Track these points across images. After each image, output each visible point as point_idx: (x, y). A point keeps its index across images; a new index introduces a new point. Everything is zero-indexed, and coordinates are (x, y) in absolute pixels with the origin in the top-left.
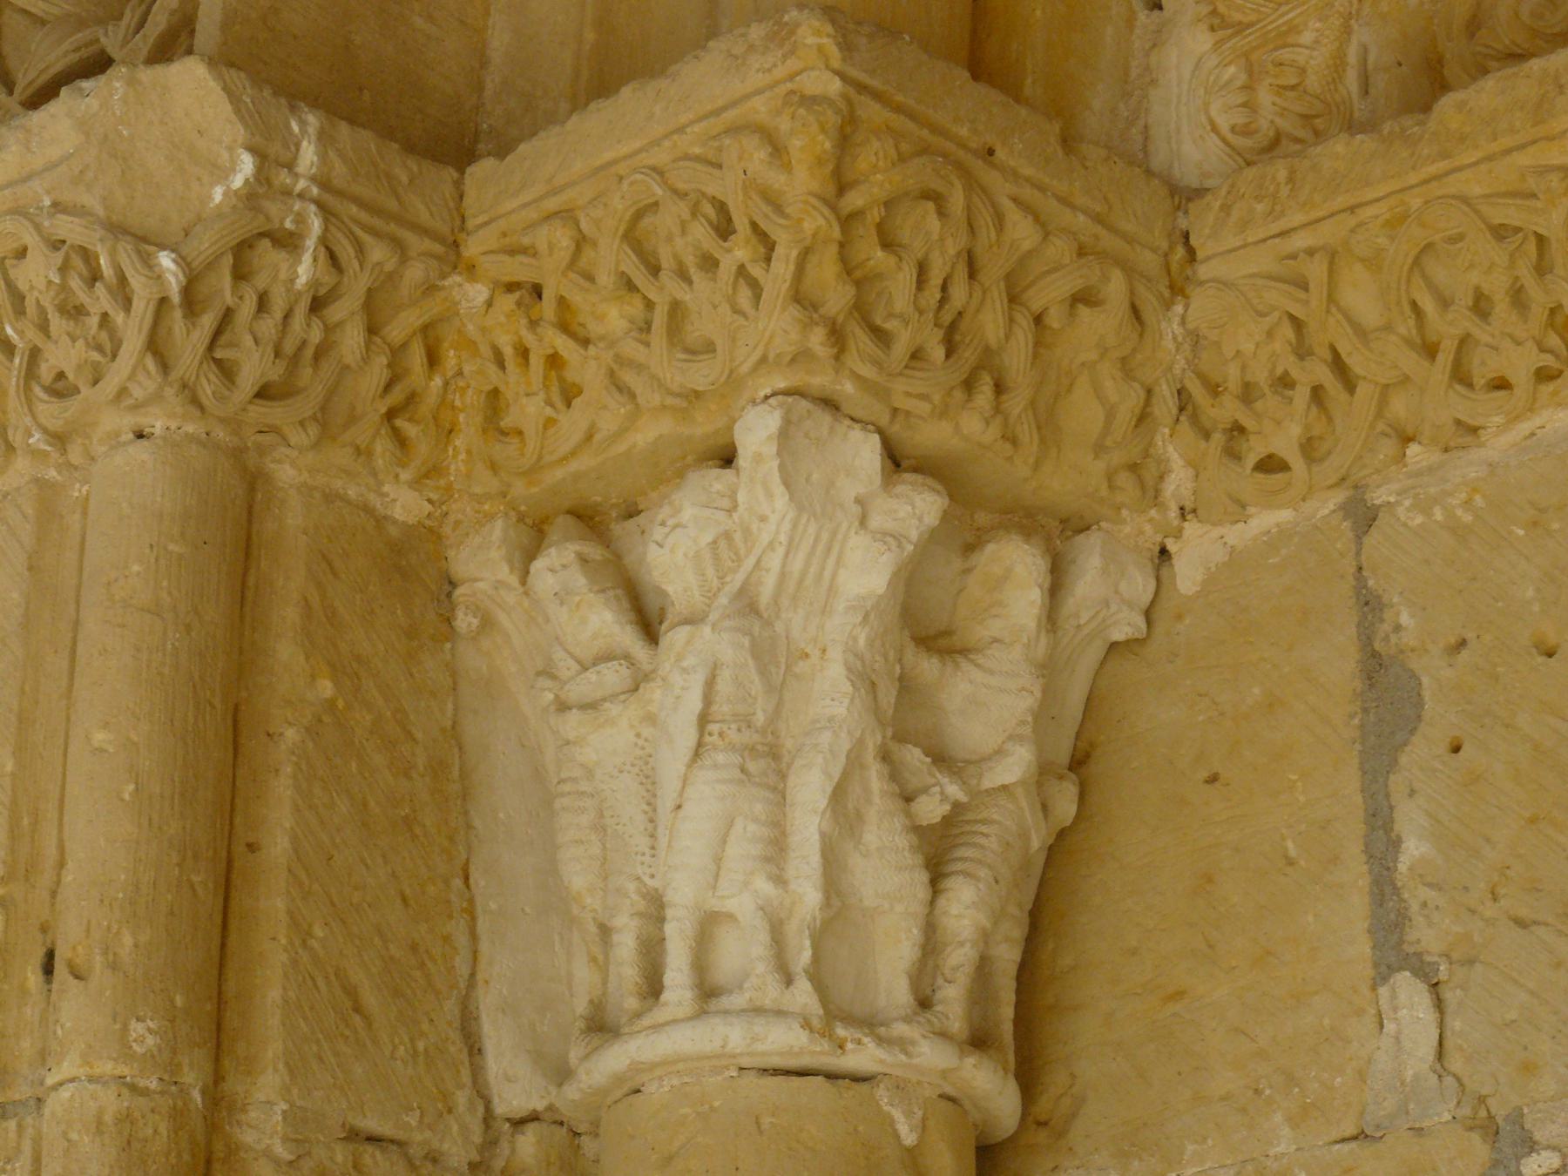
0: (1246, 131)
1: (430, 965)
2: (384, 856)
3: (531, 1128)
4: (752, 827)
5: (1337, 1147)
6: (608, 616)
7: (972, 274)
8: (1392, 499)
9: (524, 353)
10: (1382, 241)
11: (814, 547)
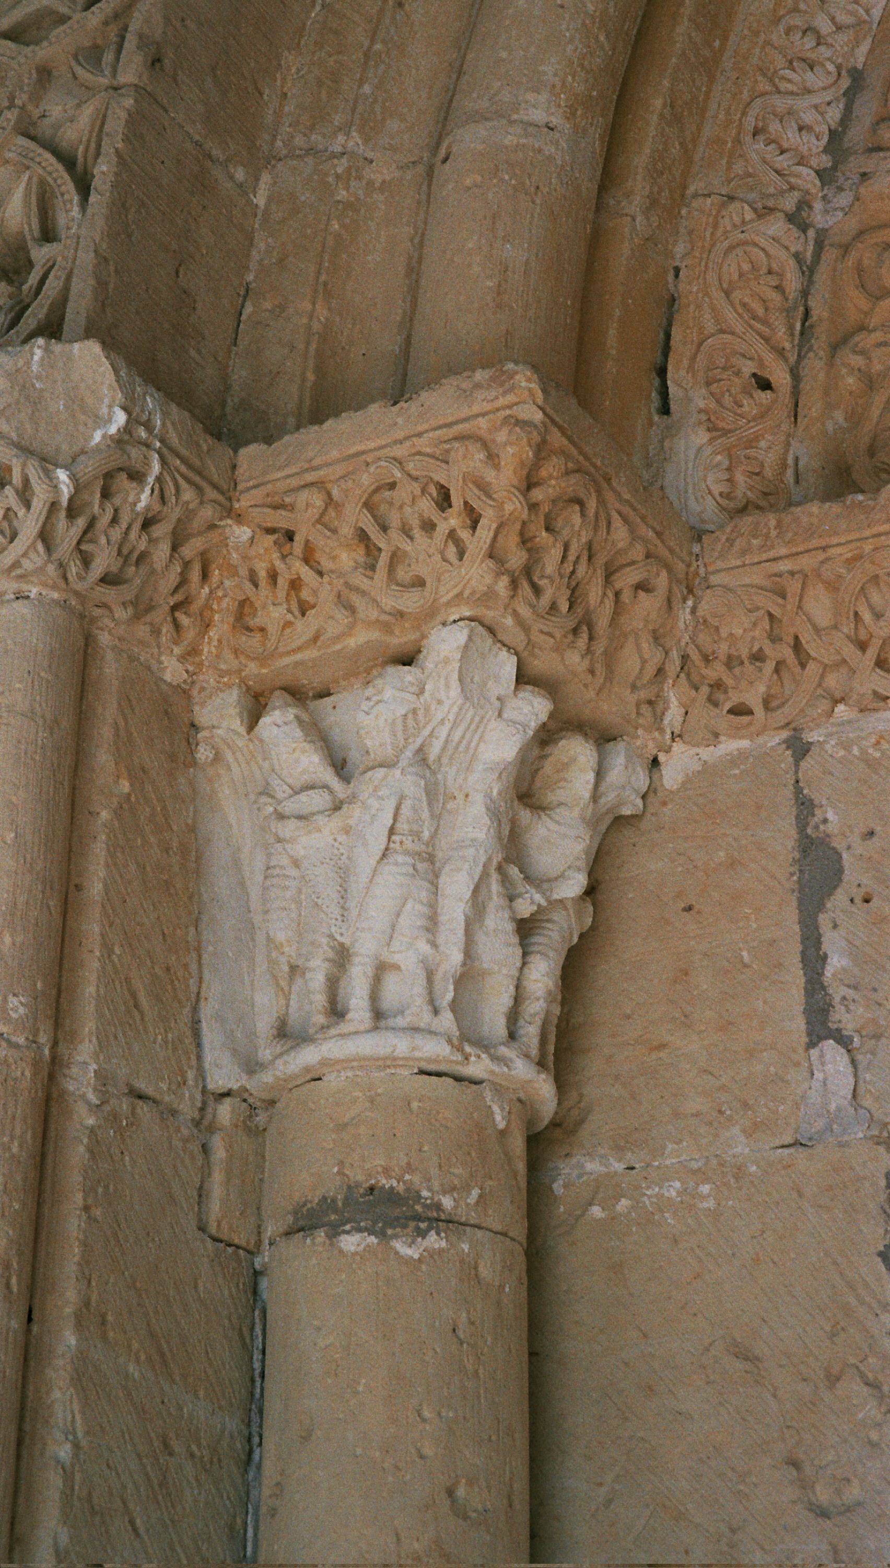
0: (728, 496)
1: (176, 982)
2: (154, 905)
3: (228, 1100)
4: (418, 907)
5: (780, 1150)
6: (316, 758)
7: (590, 558)
8: (821, 739)
9: (273, 577)
10: (843, 571)
11: (470, 724)
